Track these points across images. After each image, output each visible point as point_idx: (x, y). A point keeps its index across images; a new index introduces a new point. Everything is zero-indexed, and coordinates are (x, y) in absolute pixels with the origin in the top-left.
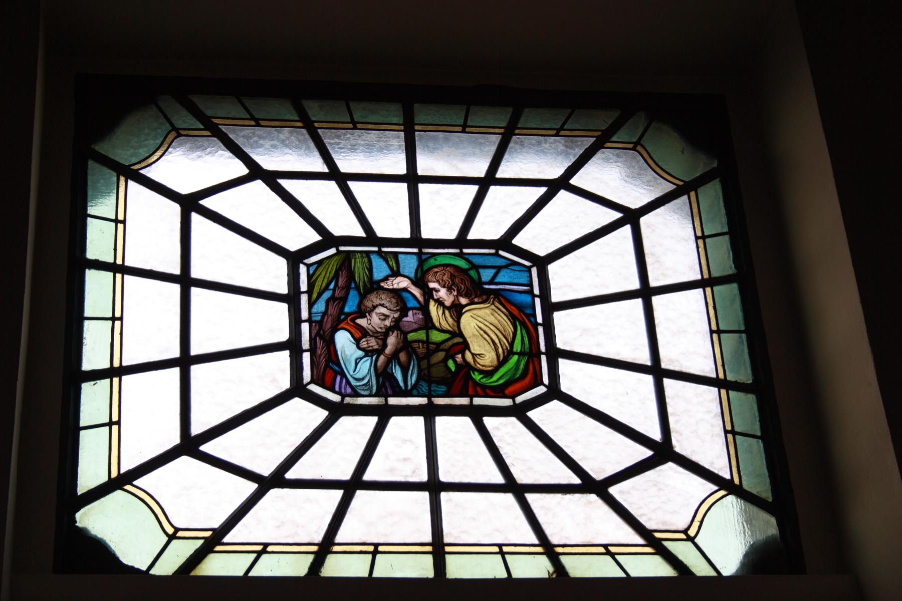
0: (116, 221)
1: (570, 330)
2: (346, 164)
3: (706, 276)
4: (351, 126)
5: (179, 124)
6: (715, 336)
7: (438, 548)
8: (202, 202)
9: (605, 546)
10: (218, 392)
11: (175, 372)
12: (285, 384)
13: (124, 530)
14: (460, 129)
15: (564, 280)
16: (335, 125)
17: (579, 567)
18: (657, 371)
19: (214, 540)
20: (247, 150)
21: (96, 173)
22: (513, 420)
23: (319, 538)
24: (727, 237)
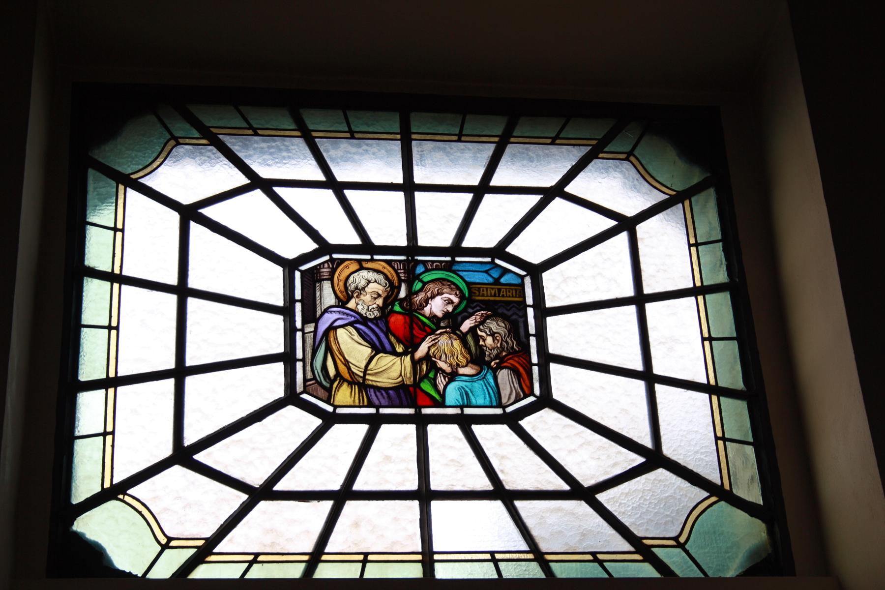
0: (115, 229)
1: (562, 335)
2: (341, 175)
3: (698, 284)
4: (348, 135)
5: (177, 134)
6: (707, 343)
7: (428, 557)
8: (202, 211)
9: (594, 554)
10: (212, 402)
11: (169, 384)
12: (280, 393)
13: (118, 536)
14: (456, 138)
15: (558, 287)
16: (333, 136)
17: (561, 571)
18: (649, 377)
19: (205, 551)
20: (248, 162)
21: (96, 183)
22: (505, 427)
23: (309, 547)
24: (720, 245)
